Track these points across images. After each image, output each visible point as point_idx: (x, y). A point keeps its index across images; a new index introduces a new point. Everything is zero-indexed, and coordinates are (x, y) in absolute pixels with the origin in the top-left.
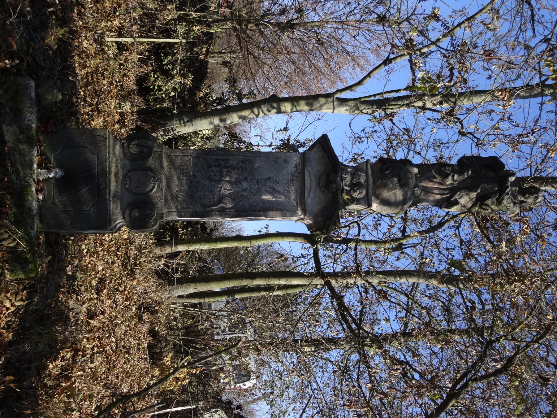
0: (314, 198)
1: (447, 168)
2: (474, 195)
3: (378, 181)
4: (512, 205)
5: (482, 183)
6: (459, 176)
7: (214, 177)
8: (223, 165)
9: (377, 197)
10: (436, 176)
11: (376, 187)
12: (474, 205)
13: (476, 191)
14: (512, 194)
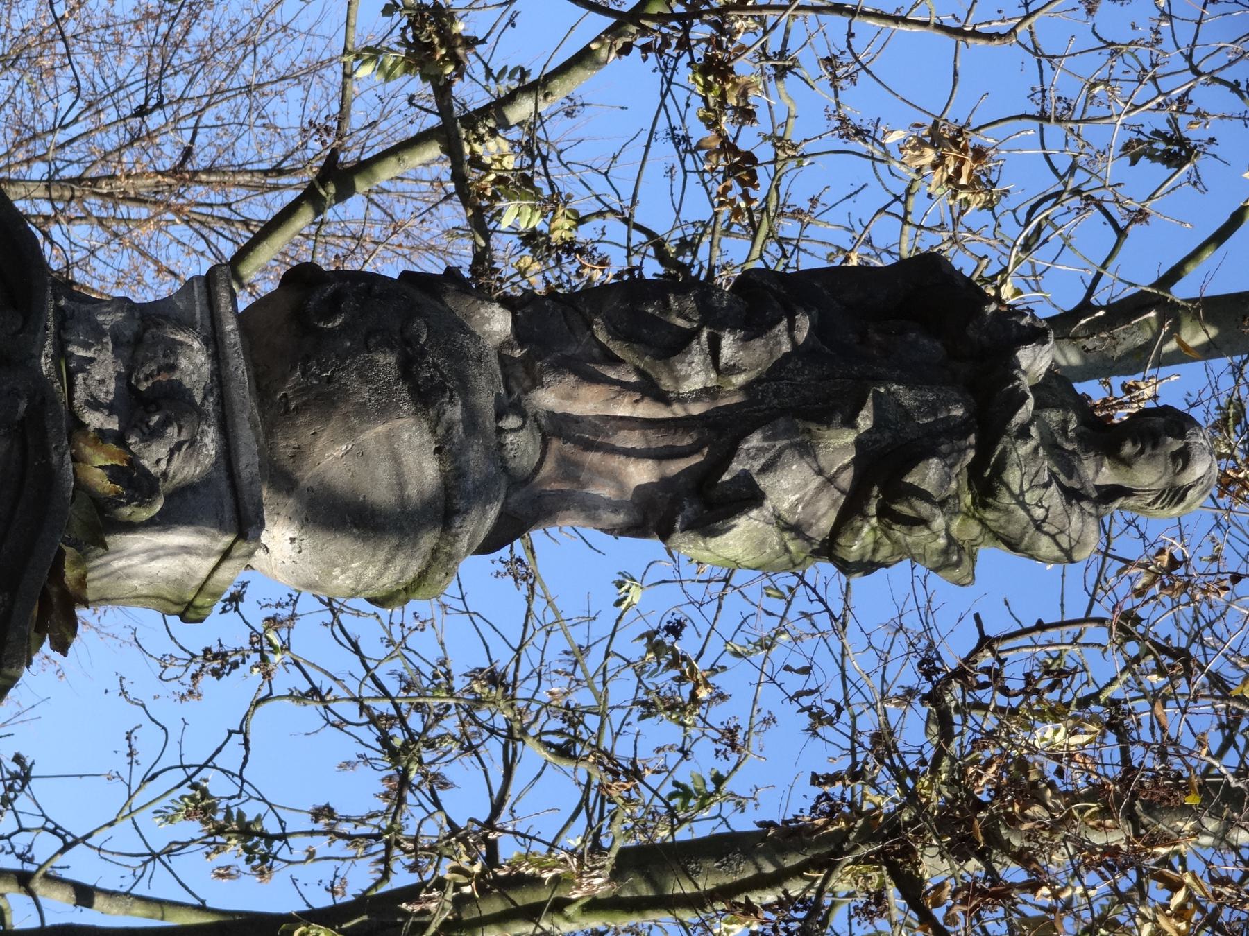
1: (675, 305)
2: (839, 447)
3: (284, 379)
4: (1054, 497)
5: (879, 380)
6: (746, 339)
9: (284, 481)
10: (617, 348)
11: (276, 414)
12: (849, 513)
13: (850, 423)
14: (1051, 446)
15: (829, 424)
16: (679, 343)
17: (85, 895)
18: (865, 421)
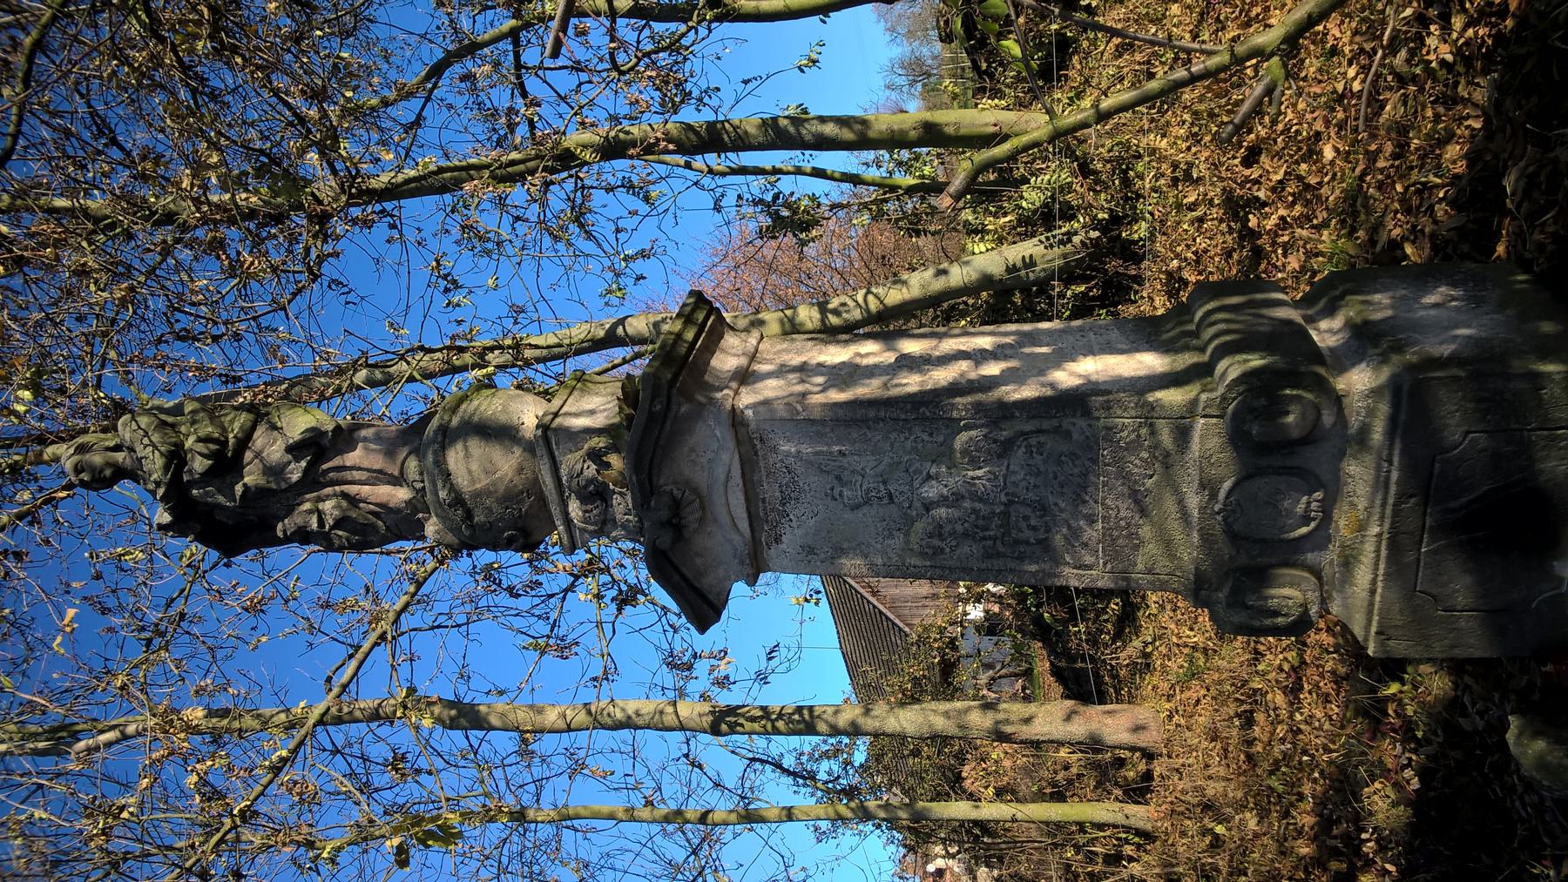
0: (710, 461)
2: (252, 477)
7: (1028, 512)
8: (999, 542)
12: (245, 441)
15: (256, 487)
16: (339, 523)
17: (688, 166)
18: (239, 489)
